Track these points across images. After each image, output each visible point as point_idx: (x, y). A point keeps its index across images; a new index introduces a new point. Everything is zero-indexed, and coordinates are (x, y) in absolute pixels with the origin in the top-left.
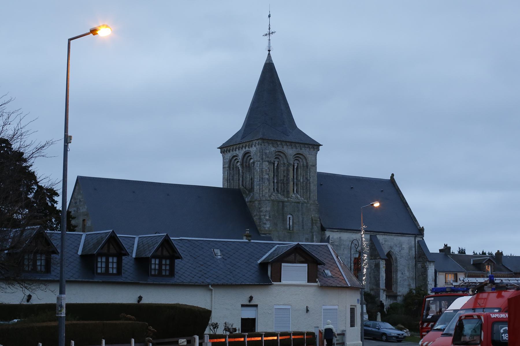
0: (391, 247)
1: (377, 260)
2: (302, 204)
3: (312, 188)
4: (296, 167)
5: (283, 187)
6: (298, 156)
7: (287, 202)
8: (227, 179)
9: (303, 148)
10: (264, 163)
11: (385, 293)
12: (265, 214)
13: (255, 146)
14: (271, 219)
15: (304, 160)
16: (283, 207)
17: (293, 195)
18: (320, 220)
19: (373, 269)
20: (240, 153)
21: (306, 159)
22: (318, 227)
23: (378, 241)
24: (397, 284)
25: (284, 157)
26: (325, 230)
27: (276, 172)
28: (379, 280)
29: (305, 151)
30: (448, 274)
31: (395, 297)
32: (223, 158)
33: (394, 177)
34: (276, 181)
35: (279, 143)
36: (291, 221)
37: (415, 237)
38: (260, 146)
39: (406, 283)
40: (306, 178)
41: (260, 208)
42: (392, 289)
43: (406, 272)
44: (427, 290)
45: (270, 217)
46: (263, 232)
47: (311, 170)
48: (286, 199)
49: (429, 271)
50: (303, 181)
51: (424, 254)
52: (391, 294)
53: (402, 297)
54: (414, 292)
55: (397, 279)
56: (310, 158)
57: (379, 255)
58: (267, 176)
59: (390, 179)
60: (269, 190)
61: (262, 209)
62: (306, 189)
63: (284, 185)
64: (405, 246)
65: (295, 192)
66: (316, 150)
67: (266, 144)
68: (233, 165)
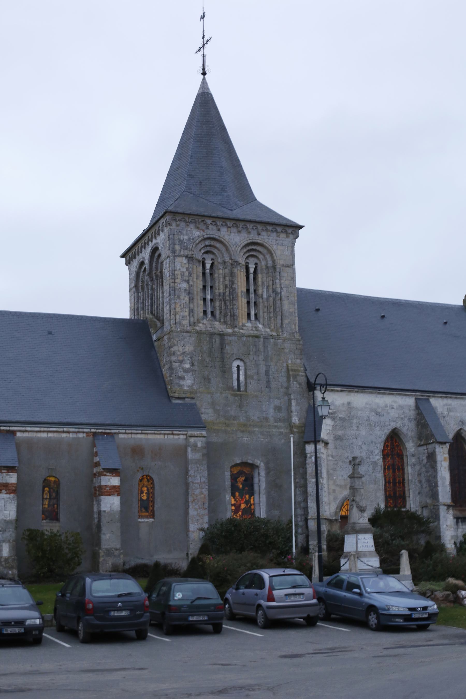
1: (430, 446)
3: (286, 307)
4: (252, 270)
5: (223, 308)
6: (252, 248)
8: (135, 310)
9: (264, 233)
10: (178, 259)
12: (181, 358)
13: (163, 231)
14: (196, 368)
15: (268, 256)
16: (222, 348)
17: (249, 324)
18: (306, 370)
19: (425, 466)
20: (146, 254)
21: (271, 254)
22: (300, 384)
23: (433, 410)
25: (223, 249)
27: (209, 276)
28: (436, 486)
29: (268, 239)
32: (130, 271)
34: (209, 297)
35: (209, 221)
36: (242, 373)
38: (169, 227)
40: (274, 291)
41: (170, 347)
45: (192, 365)
46: (176, 395)
47: (282, 274)
48: (230, 331)
50: (269, 296)
56: (279, 252)
57: (433, 436)
58: (185, 285)
59: (461, 304)
60: (191, 311)
61: (175, 348)
62: (275, 310)
63: (225, 303)
65: (253, 317)
66: (291, 236)
67: (183, 224)
68: (143, 282)
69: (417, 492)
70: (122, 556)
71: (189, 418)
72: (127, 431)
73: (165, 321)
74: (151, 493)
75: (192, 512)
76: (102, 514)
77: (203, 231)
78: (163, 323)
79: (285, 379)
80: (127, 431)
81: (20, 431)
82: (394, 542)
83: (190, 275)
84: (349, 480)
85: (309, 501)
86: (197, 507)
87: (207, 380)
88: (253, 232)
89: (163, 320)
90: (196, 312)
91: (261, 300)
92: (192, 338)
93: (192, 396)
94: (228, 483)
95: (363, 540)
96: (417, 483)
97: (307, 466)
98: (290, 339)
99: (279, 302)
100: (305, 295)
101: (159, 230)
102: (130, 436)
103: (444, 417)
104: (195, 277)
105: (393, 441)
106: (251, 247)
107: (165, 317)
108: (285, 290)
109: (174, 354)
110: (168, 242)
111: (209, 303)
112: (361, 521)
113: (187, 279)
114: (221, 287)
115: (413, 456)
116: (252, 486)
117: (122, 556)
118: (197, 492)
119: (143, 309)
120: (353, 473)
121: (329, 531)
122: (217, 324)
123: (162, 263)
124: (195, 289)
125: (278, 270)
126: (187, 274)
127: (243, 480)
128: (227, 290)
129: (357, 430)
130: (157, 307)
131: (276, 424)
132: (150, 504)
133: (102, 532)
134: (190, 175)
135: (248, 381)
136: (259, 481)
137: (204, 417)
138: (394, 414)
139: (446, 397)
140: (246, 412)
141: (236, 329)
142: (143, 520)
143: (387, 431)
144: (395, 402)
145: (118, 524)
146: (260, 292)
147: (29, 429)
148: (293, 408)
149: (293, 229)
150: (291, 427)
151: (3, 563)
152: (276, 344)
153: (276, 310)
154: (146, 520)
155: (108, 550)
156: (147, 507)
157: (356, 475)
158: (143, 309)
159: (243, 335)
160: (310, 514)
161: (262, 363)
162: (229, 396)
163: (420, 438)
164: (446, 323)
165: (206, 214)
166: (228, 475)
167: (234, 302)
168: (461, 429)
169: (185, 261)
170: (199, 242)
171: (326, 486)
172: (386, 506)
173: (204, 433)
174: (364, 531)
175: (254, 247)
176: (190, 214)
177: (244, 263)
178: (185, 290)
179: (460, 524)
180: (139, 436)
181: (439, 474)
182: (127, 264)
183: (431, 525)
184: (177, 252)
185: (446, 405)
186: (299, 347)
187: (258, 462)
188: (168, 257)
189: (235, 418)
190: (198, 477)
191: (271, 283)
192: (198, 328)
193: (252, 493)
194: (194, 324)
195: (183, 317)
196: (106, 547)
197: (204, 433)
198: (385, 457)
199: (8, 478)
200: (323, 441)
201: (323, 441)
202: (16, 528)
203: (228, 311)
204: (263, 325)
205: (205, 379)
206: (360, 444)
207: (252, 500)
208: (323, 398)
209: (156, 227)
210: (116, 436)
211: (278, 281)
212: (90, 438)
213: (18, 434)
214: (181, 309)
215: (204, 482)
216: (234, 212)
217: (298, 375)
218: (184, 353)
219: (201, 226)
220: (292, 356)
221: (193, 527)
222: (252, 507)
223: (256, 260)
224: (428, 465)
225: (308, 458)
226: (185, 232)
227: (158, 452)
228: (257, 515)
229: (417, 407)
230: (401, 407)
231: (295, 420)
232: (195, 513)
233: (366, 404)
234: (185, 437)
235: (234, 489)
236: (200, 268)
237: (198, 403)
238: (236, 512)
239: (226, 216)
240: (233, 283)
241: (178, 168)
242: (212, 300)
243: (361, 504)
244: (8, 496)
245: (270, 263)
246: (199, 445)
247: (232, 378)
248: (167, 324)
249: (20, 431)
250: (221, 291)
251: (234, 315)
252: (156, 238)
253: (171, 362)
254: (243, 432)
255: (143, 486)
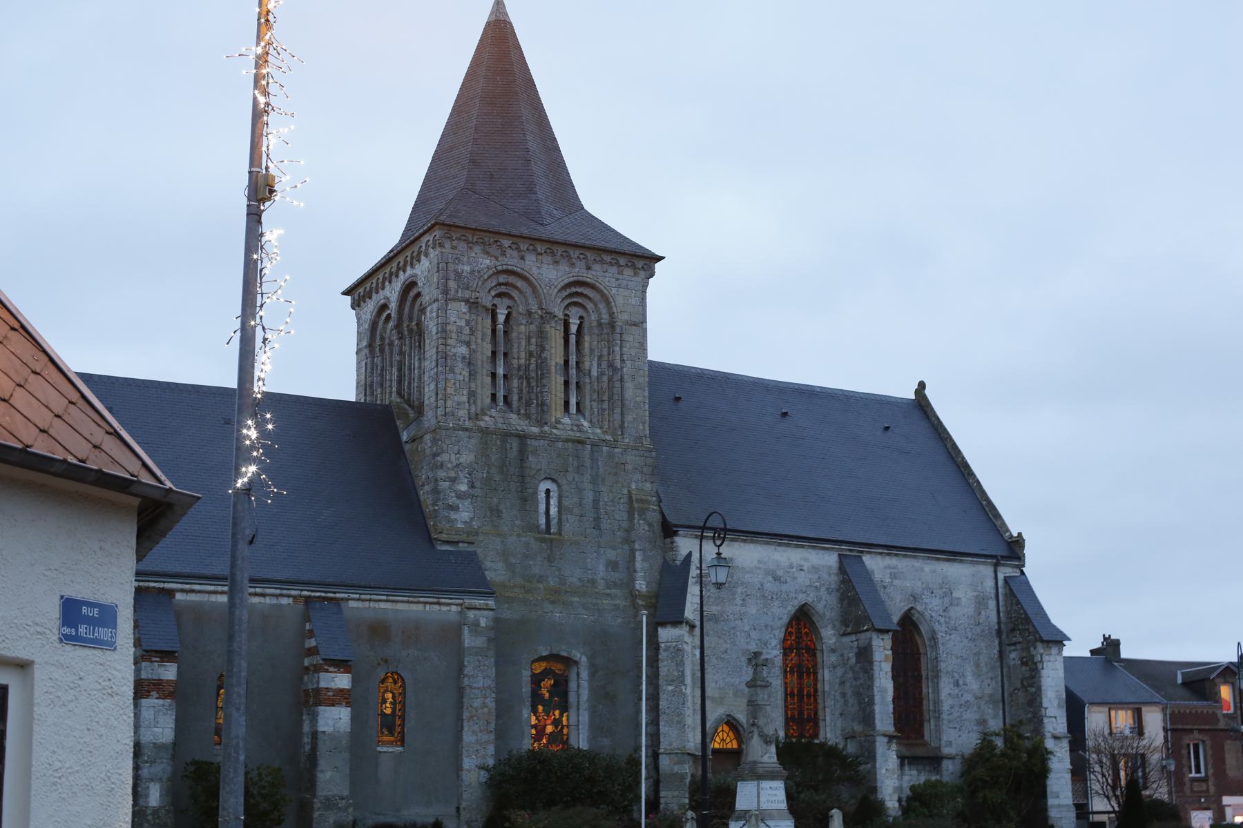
0: (915, 597)
1: (862, 636)
2: (593, 445)
3: (629, 394)
4: (574, 329)
6: (577, 291)
7: (537, 437)
8: (365, 386)
9: (596, 267)
11: (894, 747)
12: (452, 474)
13: (426, 255)
14: (477, 492)
15: (602, 306)
16: (522, 458)
17: (566, 421)
18: (660, 501)
19: (852, 668)
20: (392, 293)
21: (608, 303)
22: (650, 525)
23: (867, 575)
24: (938, 718)
25: (528, 291)
26: (675, 533)
27: (501, 337)
28: (872, 702)
29: (604, 276)
30: (1117, 709)
31: (934, 760)
32: (358, 319)
33: (928, 392)
34: (500, 371)
35: (506, 243)
36: (553, 502)
37: (996, 565)
38: (438, 249)
39: (971, 716)
40: (611, 365)
41: (435, 455)
42: (922, 736)
43: (969, 679)
44: (1043, 737)
45: (472, 486)
46: (444, 537)
47: (625, 337)
48: (535, 430)
49: (1044, 673)
50: (601, 374)
51: (1027, 620)
52: (919, 752)
53: (958, 761)
54: (999, 742)
55: (937, 702)
56: (622, 300)
57: (867, 618)
58: (463, 350)
59: (913, 397)
60: (472, 394)
61: (444, 457)
62: (611, 398)
63: (529, 383)
64: (964, 594)
65: (573, 409)
66: (642, 274)
67: (462, 246)
68: (382, 339)
69: (837, 713)
70: (351, 810)
71: (461, 575)
72: (363, 597)
73: (426, 409)
74: (400, 702)
75: (468, 737)
76: (320, 736)
77: (497, 259)
78: (420, 410)
79: (625, 515)
80: (363, 597)
81: (182, 591)
82: (802, 796)
83: (472, 333)
84: (747, 690)
85: (662, 723)
86: (476, 728)
87: (496, 512)
88: (578, 263)
89: (421, 405)
90: (479, 396)
91: (587, 380)
92: (473, 441)
93: (471, 539)
94: (526, 689)
95: (770, 792)
96: (838, 698)
97: (660, 664)
98: (634, 448)
99: (618, 384)
100: (665, 375)
101: (419, 253)
102: (366, 604)
103: (885, 587)
104: (480, 337)
105: (802, 624)
106: (574, 290)
107: (426, 402)
108: (629, 363)
109: (442, 466)
110: (436, 275)
111: (501, 381)
112: (765, 759)
113: (467, 339)
114: (523, 355)
115: (833, 651)
116: (565, 695)
117: (351, 810)
118: (477, 703)
119: (382, 385)
120: (754, 679)
121: (692, 776)
122: (513, 417)
123: (423, 310)
124: (479, 356)
125: (618, 330)
126: (467, 331)
127: (553, 687)
128: (533, 360)
129: (742, 605)
130: (410, 383)
131: (608, 591)
132: (398, 722)
133: (319, 768)
134: (473, 161)
135: (564, 517)
136: (578, 686)
137: (489, 575)
138: (803, 579)
139: (889, 554)
140: (559, 570)
141: (546, 428)
142: (385, 749)
143: (791, 609)
144: (806, 560)
145: (346, 755)
146: (587, 365)
147: (197, 587)
148: (638, 565)
149: (645, 261)
150: (633, 595)
151: (150, 818)
152: (611, 456)
153: (612, 397)
154: (391, 750)
155: (327, 799)
156: (392, 725)
157: (759, 683)
158: (382, 385)
159: (558, 439)
160: (662, 746)
161: (588, 486)
162: (532, 541)
163: (845, 622)
164: (887, 428)
165: (503, 230)
166: (526, 675)
167: (544, 381)
168: (912, 608)
169: (464, 308)
170: (489, 277)
171: (690, 698)
172: (786, 734)
173: (491, 603)
174: (771, 776)
175: (579, 290)
176: (475, 230)
177: (560, 315)
178: (464, 358)
179: (906, 768)
180: (382, 605)
181: (877, 684)
182: (353, 308)
183: (862, 768)
184: (452, 293)
185: (889, 567)
186: (650, 461)
187: (577, 655)
188: (437, 300)
189: (541, 579)
190: (480, 679)
191: (605, 352)
192: (482, 424)
193: (565, 708)
194: (477, 417)
195: (459, 404)
196: (324, 793)
197: (491, 603)
198: (786, 651)
199: (161, 670)
200: (687, 623)
201: (687, 623)
202: (173, 757)
203: (533, 397)
204: (591, 422)
205: (491, 511)
206: (747, 628)
207: (564, 719)
208: (719, 554)
209: (415, 248)
210: (343, 604)
211: (617, 349)
212: (300, 606)
213: (179, 596)
214: (456, 390)
215: (489, 687)
216: (548, 228)
217: (648, 509)
218: (458, 465)
219: (494, 250)
220: (638, 476)
221: (468, 763)
222: (565, 731)
223: (581, 312)
224: (857, 669)
225: (661, 651)
226: (465, 259)
227: (414, 632)
228: (573, 742)
229: (842, 569)
230: (815, 569)
231: (641, 585)
232: (473, 739)
233: (759, 562)
234: (459, 609)
235: (536, 699)
236: (488, 322)
237: (479, 551)
238: (537, 738)
239: (536, 235)
240: (543, 349)
241: (452, 148)
242: (505, 376)
243: (766, 731)
244: (161, 702)
245: (605, 318)
246: (483, 622)
247: (536, 511)
248: (429, 414)
249: (182, 591)
250: (522, 361)
251: (543, 404)
252: (412, 266)
253: (436, 480)
254: (553, 602)
255: (386, 691)
